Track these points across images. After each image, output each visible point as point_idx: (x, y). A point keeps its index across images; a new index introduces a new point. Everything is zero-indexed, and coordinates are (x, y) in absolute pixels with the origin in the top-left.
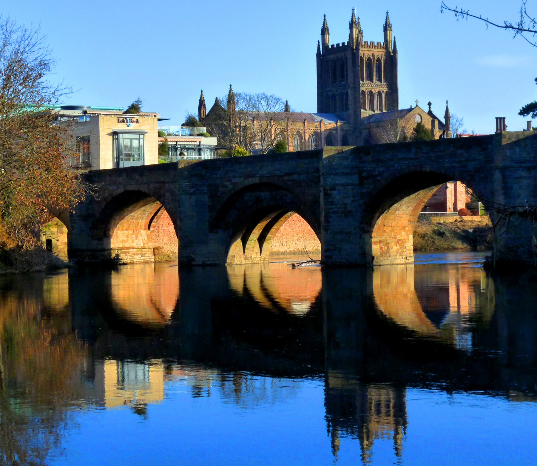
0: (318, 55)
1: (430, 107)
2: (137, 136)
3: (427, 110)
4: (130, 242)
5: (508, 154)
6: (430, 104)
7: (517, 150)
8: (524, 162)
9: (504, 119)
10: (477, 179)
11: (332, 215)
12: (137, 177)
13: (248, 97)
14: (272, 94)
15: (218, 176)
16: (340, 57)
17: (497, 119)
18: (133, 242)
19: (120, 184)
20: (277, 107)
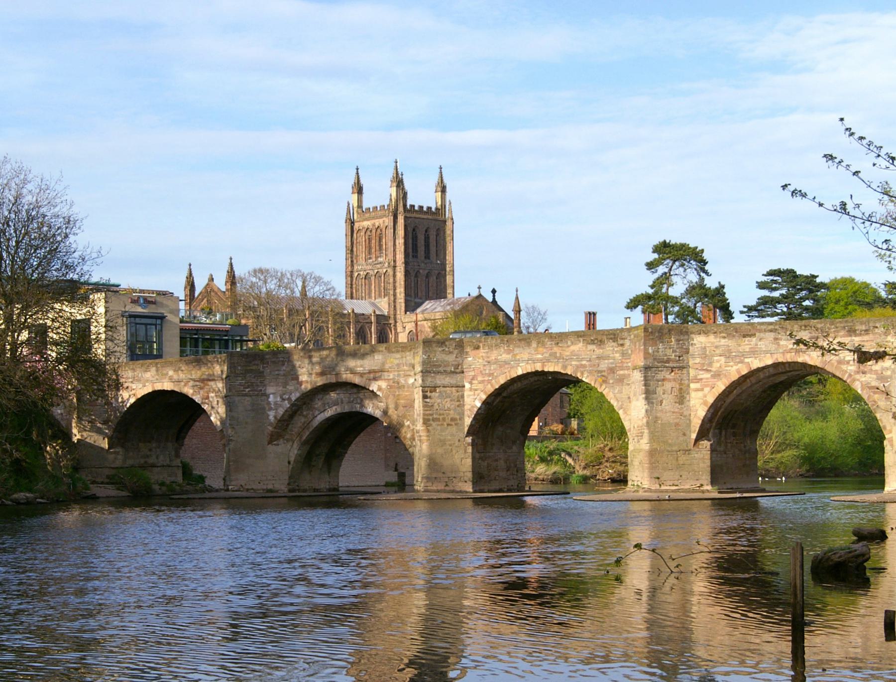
1: (494, 296)
2: (153, 321)
3: (490, 299)
4: (154, 457)
5: (650, 351)
6: (494, 291)
7: (59, 411)
8: (668, 361)
9: (594, 314)
10: (611, 381)
11: (431, 422)
12: (171, 373)
13: (279, 274)
14: (310, 271)
15: (282, 373)
16: (377, 224)
17: (586, 314)
18: (157, 458)
19: (147, 381)
20: (317, 288)
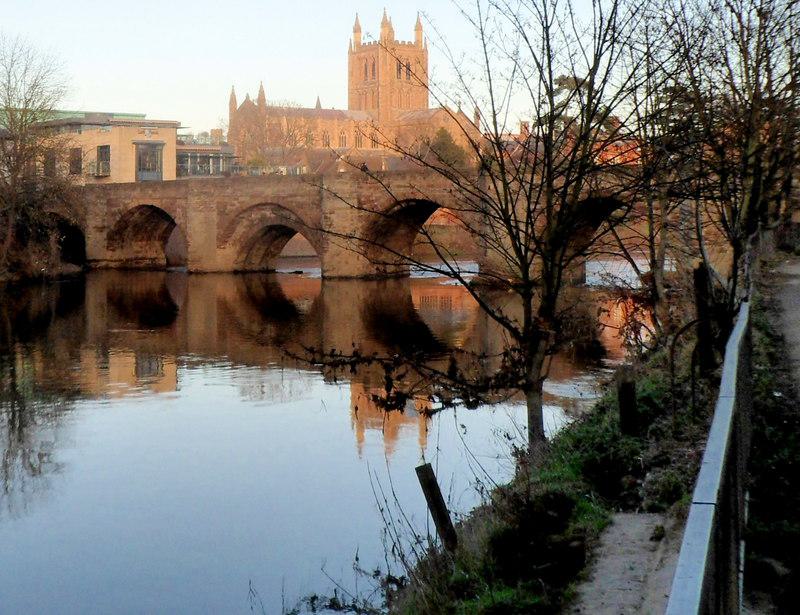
0: (351, 53)
